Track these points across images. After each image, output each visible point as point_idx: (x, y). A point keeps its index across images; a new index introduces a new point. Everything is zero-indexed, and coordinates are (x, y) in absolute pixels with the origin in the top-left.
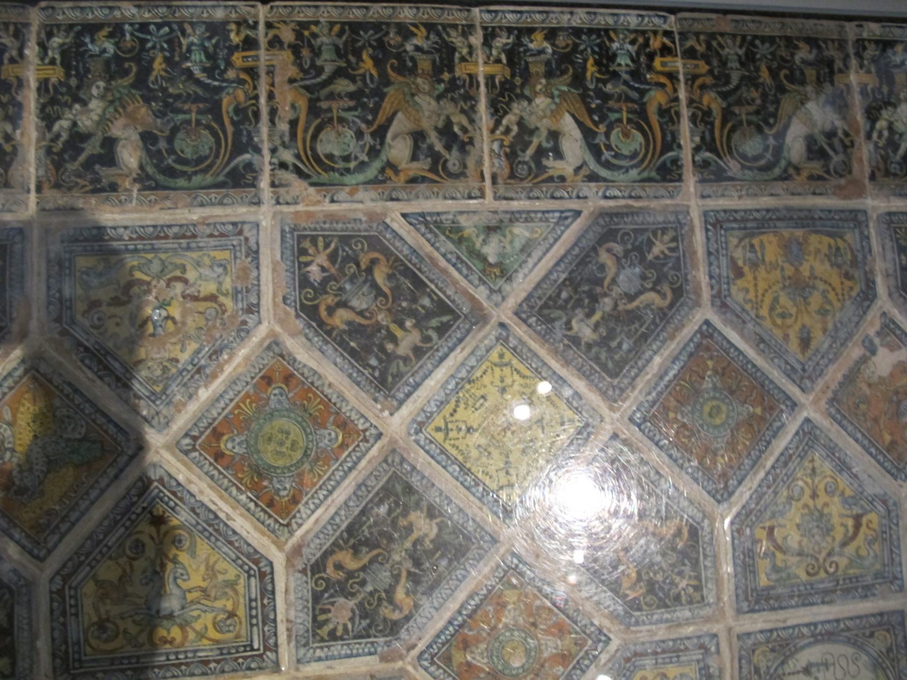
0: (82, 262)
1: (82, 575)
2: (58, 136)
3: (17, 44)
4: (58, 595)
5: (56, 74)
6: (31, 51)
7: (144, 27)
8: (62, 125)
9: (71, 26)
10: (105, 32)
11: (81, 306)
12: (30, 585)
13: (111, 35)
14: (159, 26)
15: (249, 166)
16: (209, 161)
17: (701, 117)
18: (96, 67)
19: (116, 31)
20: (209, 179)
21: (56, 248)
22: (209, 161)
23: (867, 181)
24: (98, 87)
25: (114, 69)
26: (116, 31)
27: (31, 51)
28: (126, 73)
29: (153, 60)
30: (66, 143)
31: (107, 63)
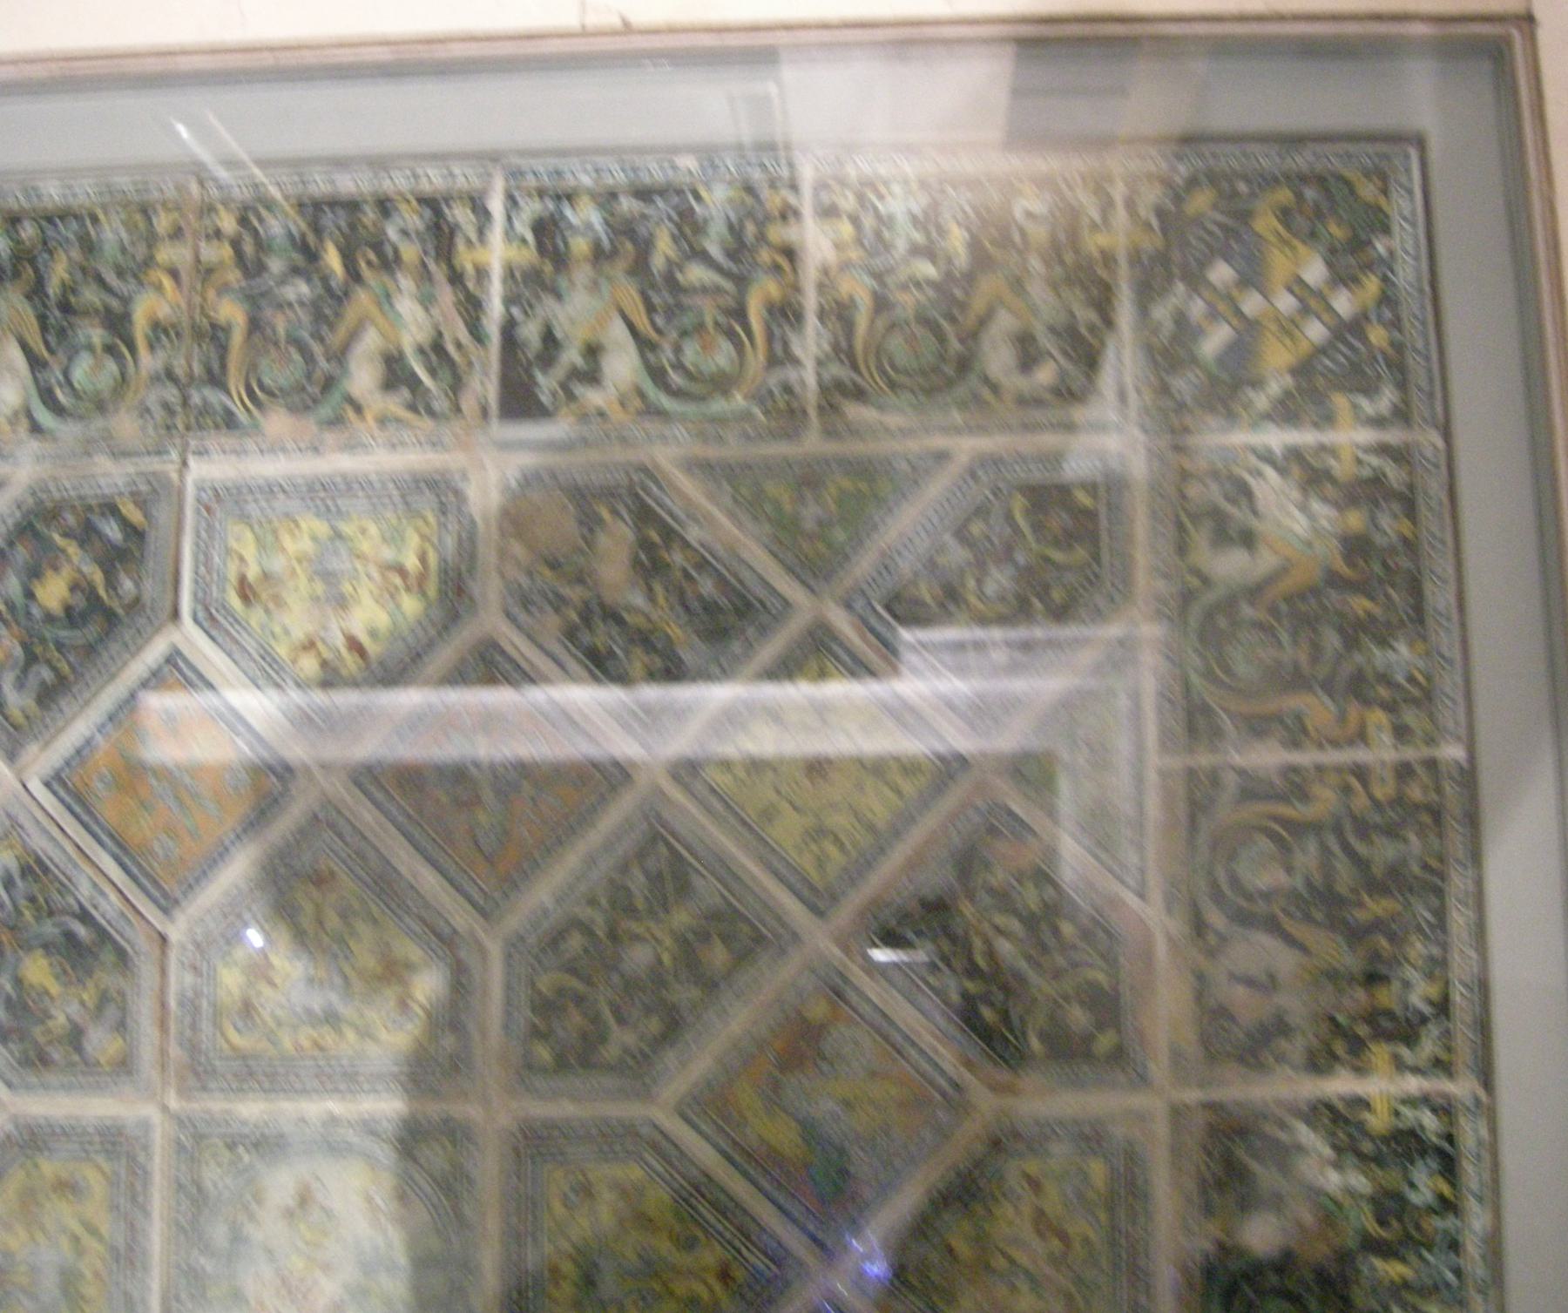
0: (1097, 1170)
1: (654, 1163)
2: (1283, 1125)
3: (1421, 1064)
4: (630, 1130)
5: (1378, 1121)
6: (1413, 1084)
7: (1454, 1246)
8: (1305, 1134)
9: (1450, 1138)
10: (1446, 1190)
11: (1032, 1167)
12: (645, 1094)
13: (1441, 1198)
14: (1458, 1272)
15: (1217, 733)
16: (1226, 679)
17: (1296, 785)
18: (1391, 1178)
19: (1447, 1206)
20: (1195, 679)
21: (1119, 1132)
22: (1226, 679)
23: (1073, 1290)
24: (1360, 1182)
25: (1389, 1205)
26: (1447, 1206)
27: (1413, 1084)
28: (1382, 1222)
29: (1403, 1260)
30: (1277, 1142)
31: (1400, 1198)
